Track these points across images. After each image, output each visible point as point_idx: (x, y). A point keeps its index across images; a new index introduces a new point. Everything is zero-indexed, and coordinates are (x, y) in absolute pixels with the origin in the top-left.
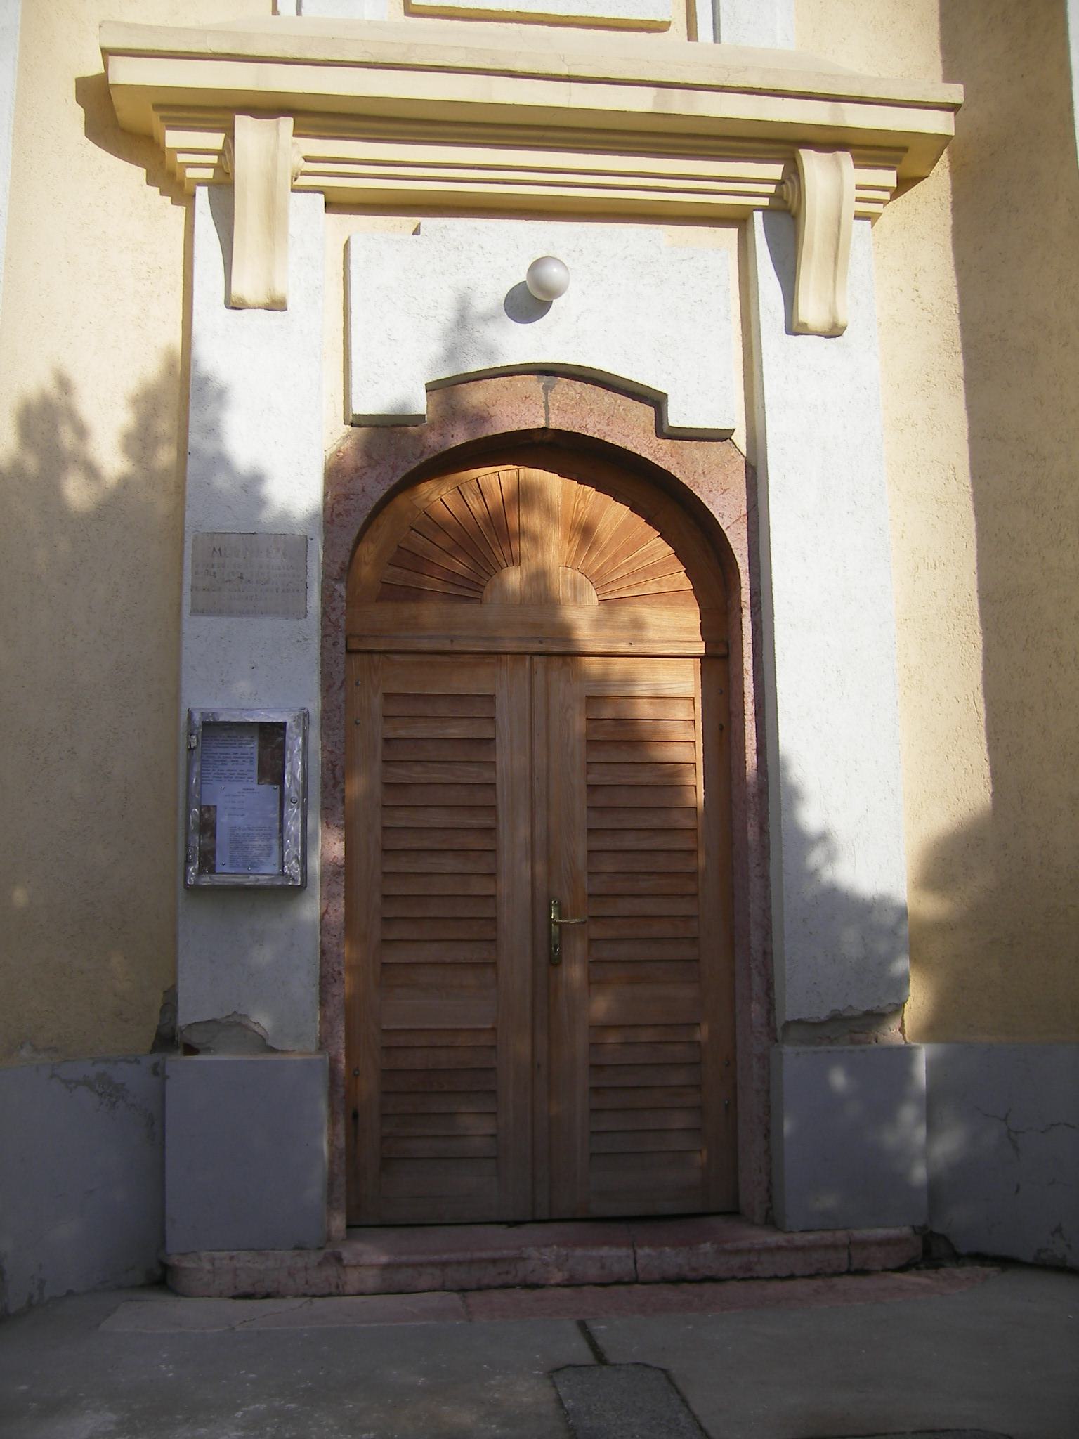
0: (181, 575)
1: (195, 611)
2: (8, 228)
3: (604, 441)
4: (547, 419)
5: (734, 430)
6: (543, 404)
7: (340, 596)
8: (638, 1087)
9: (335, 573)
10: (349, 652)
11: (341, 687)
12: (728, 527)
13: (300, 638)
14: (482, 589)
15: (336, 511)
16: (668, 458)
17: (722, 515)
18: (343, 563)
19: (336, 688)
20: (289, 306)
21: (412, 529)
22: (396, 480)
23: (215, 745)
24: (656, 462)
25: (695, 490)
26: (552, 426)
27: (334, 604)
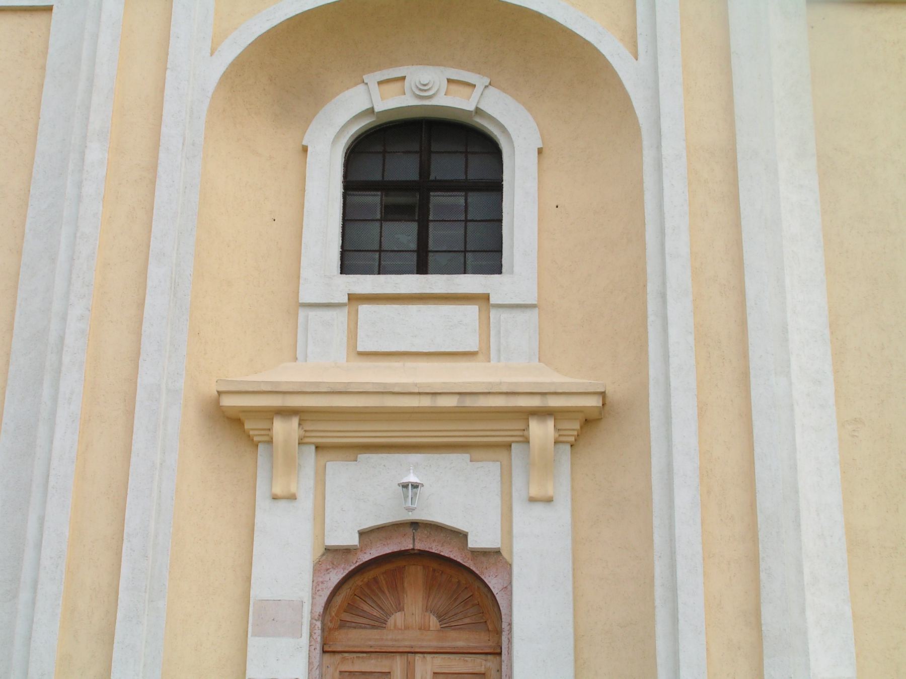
0: (248, 618)
1: (254, 635)
2: (701, 495)
3: (440, 554)
4: (414, 545)
5: (405, 76)
6: (412, 538)
7: (318, 627)
8: (489, 393)
9: (316, 617)
10: (324, 652)
11: (317, 669)
12: (497, 594)
13: (298, 647)
14: (386, 622)
15: (317, 589)
16: (470, 561)
17: (494, 588)
18: (320, 613)
19: (315, 668)
20: (297, 497)
21: (355, 595)
22: (345, 574)
23: (313, 648)
24: (464, 563)
25: (482, 573)
26: (416, 548)
27: (315, 631)
